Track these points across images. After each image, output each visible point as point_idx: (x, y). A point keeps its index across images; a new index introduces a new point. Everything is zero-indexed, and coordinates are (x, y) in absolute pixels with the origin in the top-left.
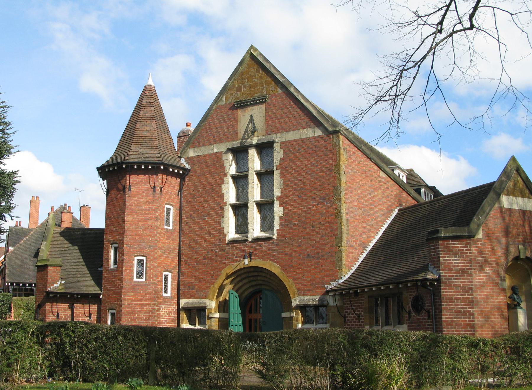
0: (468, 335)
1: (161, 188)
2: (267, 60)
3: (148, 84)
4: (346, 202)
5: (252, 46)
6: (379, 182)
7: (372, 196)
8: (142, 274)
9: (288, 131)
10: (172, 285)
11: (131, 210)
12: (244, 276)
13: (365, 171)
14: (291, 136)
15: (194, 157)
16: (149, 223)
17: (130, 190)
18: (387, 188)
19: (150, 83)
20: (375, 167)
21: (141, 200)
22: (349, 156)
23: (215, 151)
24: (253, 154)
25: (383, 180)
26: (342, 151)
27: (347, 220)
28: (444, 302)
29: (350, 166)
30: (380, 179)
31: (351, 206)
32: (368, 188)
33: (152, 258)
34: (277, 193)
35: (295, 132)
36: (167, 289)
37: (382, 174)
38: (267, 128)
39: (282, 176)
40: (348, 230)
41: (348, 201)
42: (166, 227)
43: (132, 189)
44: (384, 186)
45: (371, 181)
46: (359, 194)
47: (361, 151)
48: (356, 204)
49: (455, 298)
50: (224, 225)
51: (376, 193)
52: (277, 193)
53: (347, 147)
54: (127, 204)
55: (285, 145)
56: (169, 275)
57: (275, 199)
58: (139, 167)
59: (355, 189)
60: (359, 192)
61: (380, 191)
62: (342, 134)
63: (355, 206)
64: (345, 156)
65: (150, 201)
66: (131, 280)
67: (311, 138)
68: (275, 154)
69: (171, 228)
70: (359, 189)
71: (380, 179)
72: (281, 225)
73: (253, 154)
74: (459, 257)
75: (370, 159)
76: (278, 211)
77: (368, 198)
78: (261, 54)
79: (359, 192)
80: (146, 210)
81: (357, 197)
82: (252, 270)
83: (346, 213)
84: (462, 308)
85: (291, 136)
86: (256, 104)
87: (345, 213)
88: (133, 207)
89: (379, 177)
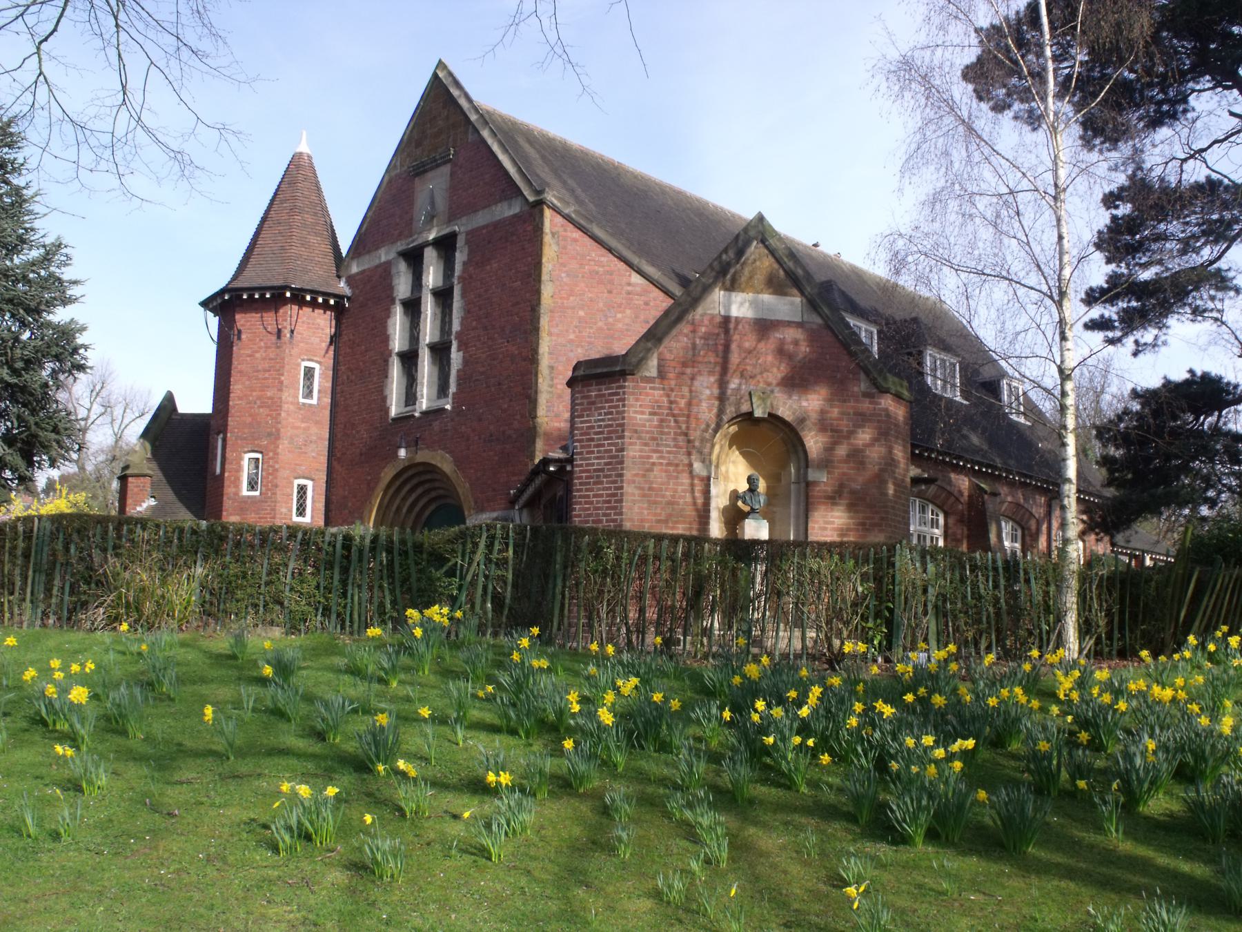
0: (500, 551)
1: (292, 332)
2: (457, 84)
3: (298, 150)
4: (550, 334)
5: (440, 61)
6: (629, 293)
7: (611, 320)
8: (256, 483)
9: (476, 211)
10: (313, 501)
11: (241, 372)
12: (415, 481)
13: (597, 273)
14: (481, 219)
15: (357, 274)
16: (269, 394)
17: (239, 338)
18: (646, 304)
19: (304, 148)
20: (622, 265)
21: (258, 355)
22: (565, 248)
23: (383, 259)
24: (430, 254)
25: (638, 289)
26: (547, 239)
27: (551, 368)
28: (577, 503)
29: (563, 265)
30: (629, 288)
31: (561, 340)
32: (601, 305)
33: (271, 454)
34: (456, 326)
35: (486, 211)
36: (304, 510)
37: (636, 278)
38: (450, 208)
39: (464, 294)
40: (551, 386)
41: (555, 330)
42: (302, 400)
43: (243, 336)
44: (639, 301)
45: (610, 292)
46: (580, 318)
47: (590, 237)
48: (572, 336)
49: (595, 496)
50: (387, 392)
51: (619, 316)
52: (456, 326)
53: (561, 230)
54: (235, 363)
55: (471, 234)
56: (309, 484)
57: (453, 337)
58: (314, 300)
59: (573, 308)
60: (581, 313)
61: (628, 312)
62: (549, 207)
63: (571, 341)
64: (555, 248)
65: (272, 355)
66: (237, 494)
67: (505, 220)
68: (457, 254)
69: (314, 401)
70: (582, 308)
71: (629, 288)
72: (459, 385)
73: (430, 254)
74: (606, 414)
75: (610, 250)
76: (456, 357)
77: (600, 324)
78: (450, 74)
79: (581, 313)
80: (265, 371)
81: (575, 323)
82: (421, 469)
83: (550, 353)
84: (605, 515)
85: (481, 219)
86: (438, 166)
87: (546, 355)
88: (243, 367)
89: (629, 284)
